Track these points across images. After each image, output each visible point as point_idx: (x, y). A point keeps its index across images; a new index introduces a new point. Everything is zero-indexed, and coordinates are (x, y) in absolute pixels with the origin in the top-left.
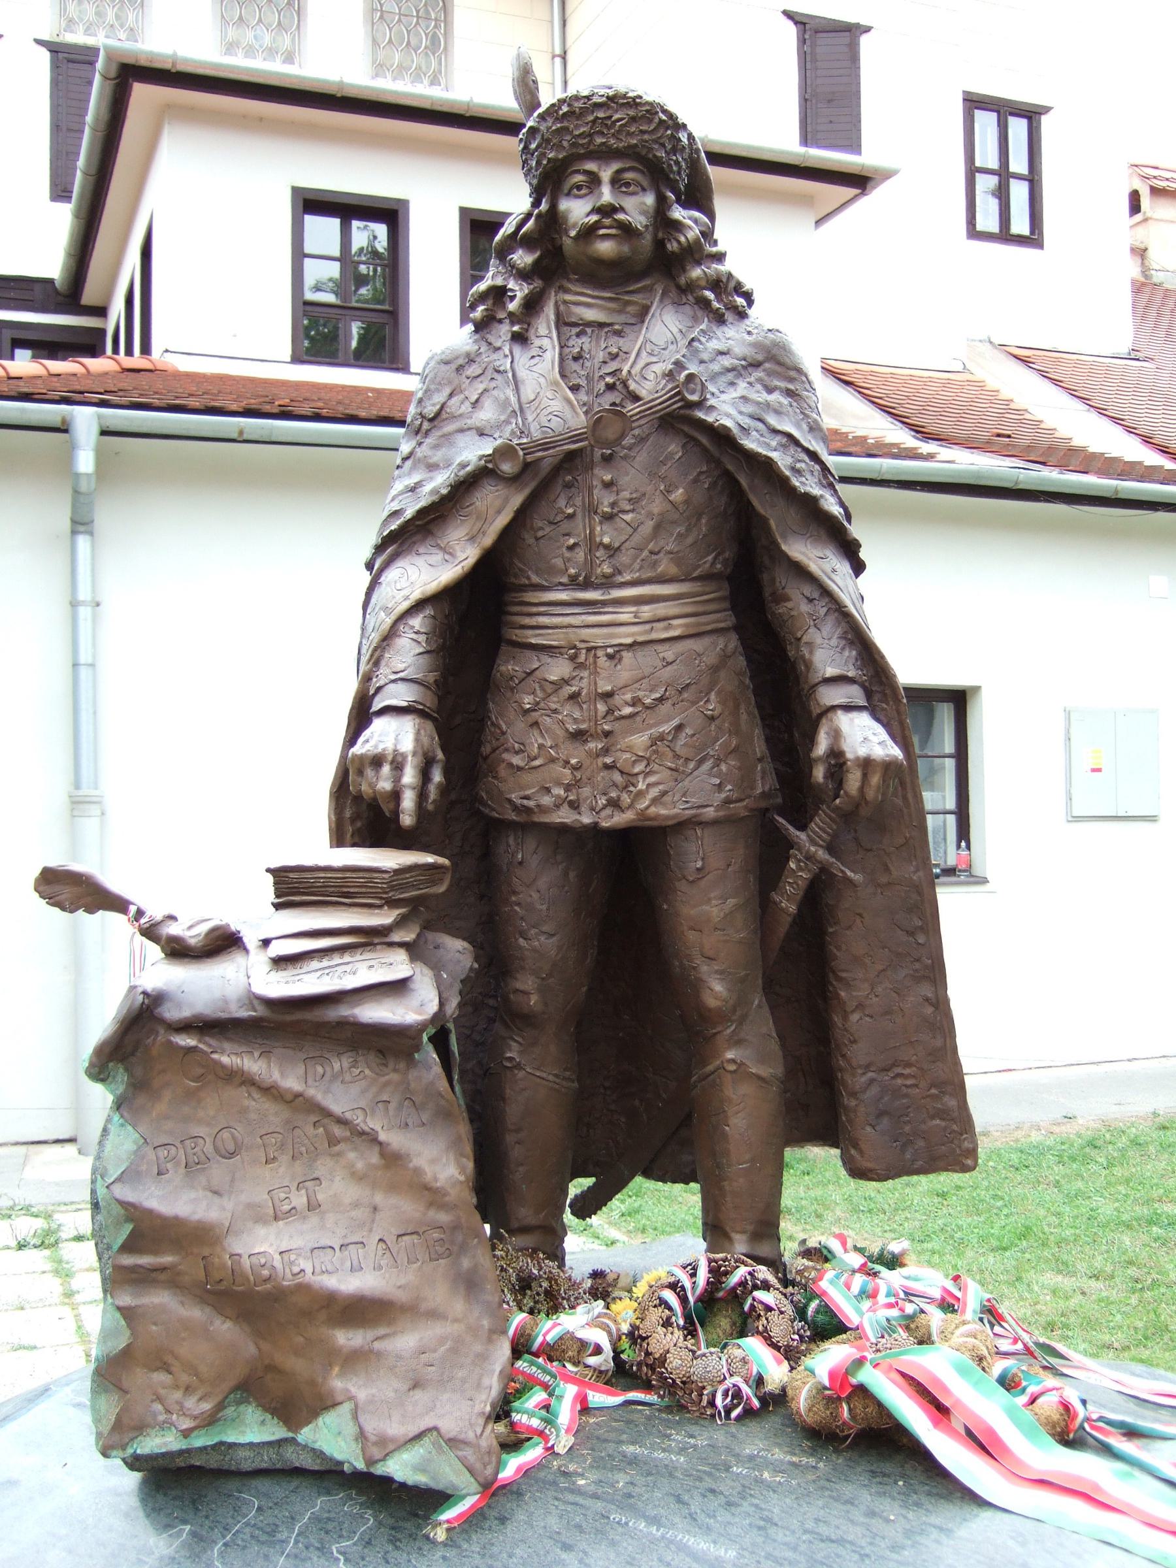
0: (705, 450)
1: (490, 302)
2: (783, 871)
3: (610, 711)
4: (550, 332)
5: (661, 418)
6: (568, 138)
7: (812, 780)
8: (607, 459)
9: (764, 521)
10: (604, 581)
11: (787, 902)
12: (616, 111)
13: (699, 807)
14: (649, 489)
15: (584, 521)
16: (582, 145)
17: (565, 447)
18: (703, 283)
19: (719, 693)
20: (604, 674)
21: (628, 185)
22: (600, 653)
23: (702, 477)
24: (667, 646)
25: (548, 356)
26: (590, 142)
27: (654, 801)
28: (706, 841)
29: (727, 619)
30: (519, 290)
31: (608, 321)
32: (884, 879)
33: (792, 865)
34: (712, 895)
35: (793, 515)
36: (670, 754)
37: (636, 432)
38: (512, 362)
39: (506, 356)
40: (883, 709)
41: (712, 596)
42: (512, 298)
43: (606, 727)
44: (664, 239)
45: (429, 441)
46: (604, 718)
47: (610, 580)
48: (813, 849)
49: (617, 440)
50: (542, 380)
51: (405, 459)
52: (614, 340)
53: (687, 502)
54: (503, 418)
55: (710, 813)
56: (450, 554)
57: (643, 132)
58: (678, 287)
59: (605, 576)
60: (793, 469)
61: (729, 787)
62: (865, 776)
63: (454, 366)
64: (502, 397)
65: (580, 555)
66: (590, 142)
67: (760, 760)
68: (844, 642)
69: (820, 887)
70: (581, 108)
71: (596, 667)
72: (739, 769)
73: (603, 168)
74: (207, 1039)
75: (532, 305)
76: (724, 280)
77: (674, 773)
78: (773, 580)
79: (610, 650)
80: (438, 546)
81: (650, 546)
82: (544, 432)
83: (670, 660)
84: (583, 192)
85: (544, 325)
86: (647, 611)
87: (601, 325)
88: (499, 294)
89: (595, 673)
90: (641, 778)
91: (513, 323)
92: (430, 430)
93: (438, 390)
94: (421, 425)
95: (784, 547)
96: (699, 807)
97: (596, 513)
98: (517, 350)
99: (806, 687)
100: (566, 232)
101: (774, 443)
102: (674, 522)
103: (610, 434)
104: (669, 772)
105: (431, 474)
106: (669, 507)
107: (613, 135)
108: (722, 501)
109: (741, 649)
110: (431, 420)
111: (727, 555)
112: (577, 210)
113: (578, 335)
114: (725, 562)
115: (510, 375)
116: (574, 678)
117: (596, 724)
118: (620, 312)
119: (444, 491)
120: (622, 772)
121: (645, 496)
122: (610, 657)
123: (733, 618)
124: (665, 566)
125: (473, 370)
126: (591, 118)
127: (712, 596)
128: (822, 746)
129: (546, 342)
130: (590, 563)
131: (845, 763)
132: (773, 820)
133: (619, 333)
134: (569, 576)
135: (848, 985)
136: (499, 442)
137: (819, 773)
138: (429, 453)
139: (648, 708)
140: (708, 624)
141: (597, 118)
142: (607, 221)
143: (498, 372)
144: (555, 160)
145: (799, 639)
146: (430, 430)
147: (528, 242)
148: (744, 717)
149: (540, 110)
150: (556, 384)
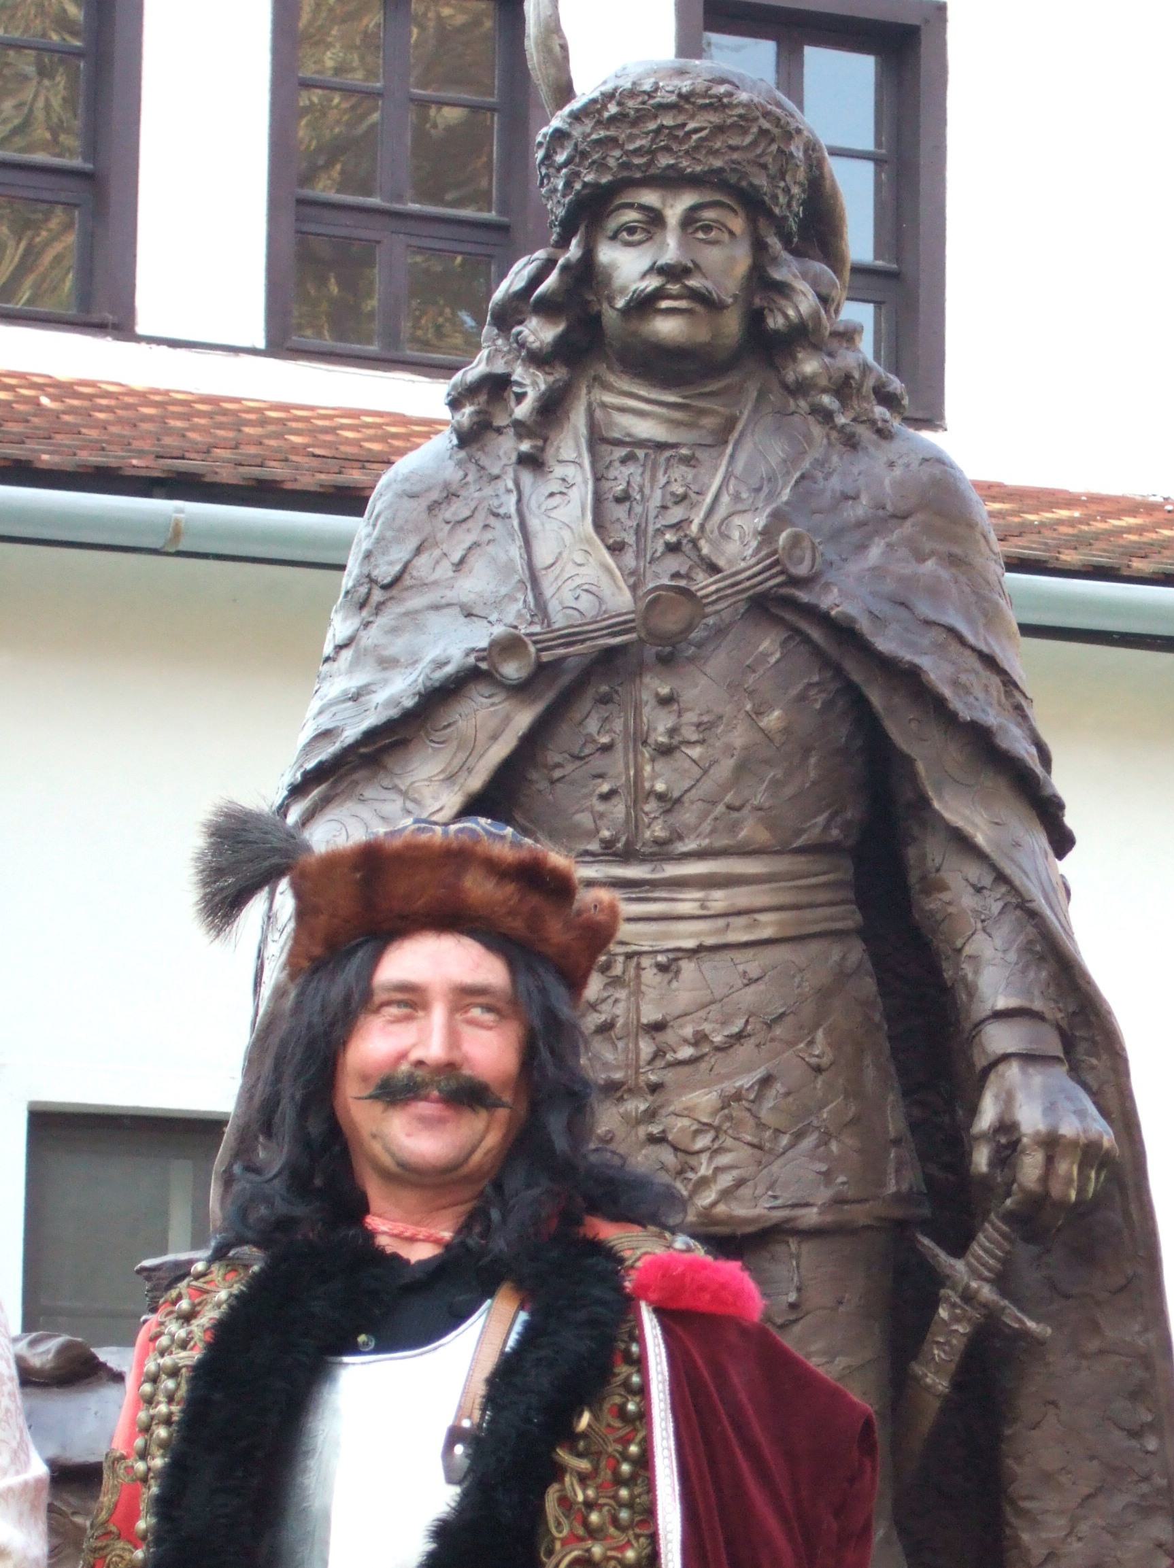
0: (816, 651)
1: (483, 398)
2: (928, 1325)
3: (659, 1054)
4: (580, 455)
5: (750, 598)
6: (617, 153)
7: (973, 1169)
8: (667, 661)
9: (908, 761)
10: (655, 849)
11: (935, 1376)
12: (692, 117)
13: (794, 1206)
14: (728, 710)
15: (626, 755)
16: (638, 167)
17: (601, 642)
18: (823, 382)
19: (828, 1033)
20: (651, 994)
21: (707, 228)
22: (646, 962)
23: (812, 692)
24: (750, 953)
25: (574, 494)
26: (650, 163)
27: (726, 1194)
28: (804, 1260)
29: (851, 918)
30: (532, 385)
31: (672, 439)
32: (1093, 1345)
33: (943, 1313)
34: (813, 1348)
35: (954, 754)
36: (751, 1122)
37: (711, 621)
38: (519, 501)
39: (509, 491)
40: (1093, 1068)
41: (822, 879)
42: (520, 397)
43: (653, 1078)
44: (763, 309)
45: (383, 620)
46: (650, 1063)
47: (665, 848)
48: (974, 1285)
49: (681, 632)
50: (566, 534)
51: (339, 648)
52: (679, 471)
53: (787, 731)
54: (504, 590)
55: (811, 1217)
56: (415, 801)
57: (733, 149)
58: (785, 386)
59: (657, 842)
60: (955, 683)
61: (841, 1179)
62: (1050, 1160)
63: (424, 503)
64: (503, 557)
65: (618, 809)
66: (650, 163)
67: (897, 1142)
68: (1029, 956)
69: (991, 1363)
70: (637, 110)
71: (639, 984)
72: (860, 1151)
73: (670, 201)
74: (65, 1496)
75: (552, 409)
76: (857, 375)
77: (756, 1151)
78: (923, 857)
79: (661, 958)
80: (395, 788)
81: (728, 798)
82: (568, 617)
83: (754, 975)
84: (636, 237)
85: (571, 443)
86: (720, 899)
87: (661, 446)
88: (496, 387)
89: (637, 993)
90: (704, 1158)
91: (520, 437)
92: (383, 603)
93: (397, 540)
94: (369, 594)
95: (936, 805)
96: (794, 1206)
97: (645, 743)
98: (527, 478)
99: (967, 1026)
100: (611, 300)
101: (925, 642)
102: (767, 762)
103: (670, 622)
104: (749, 1150)
105: (386, 674)
106: (759, 737)
107: (687, 152)
108: (841, 732)
109: (869, 965)
110: (385, 587)
111: (849, 815)
112: (628, 266)
113: (624, 461)
114: (846, 826)
115: (516, 523)
116: (604, 1000)
117: (637, 1073)
118: (690, 425)
119: (409, 703)
120: (676, 1149)
121: (719, 727)
122: (663, 968)
123: (858, 917)
124: (750, 830)
125: (457, 509)
126: (652, 126)
127: (822, 879)
128: (988, 1115)
129: (570, 471)
130: (634, 823)
131: (1018, 1141)
132: (914, 1248)
133: (688, 461)
134: (602, 841)
135: (1034, 1523)
136: (499, 630)
137: (981, 1159)
138: (383, 640)
139: (718, 1049)
140: (816, 922)
141: (662, 127)
142: (674, 288)
143: (496, 515)
144: (596, 185)
145: (959, 951)
146: (383, 603)
147: (548, 308)
148: (870, 1073)
149: (575, 105)
150: (588, 541)
